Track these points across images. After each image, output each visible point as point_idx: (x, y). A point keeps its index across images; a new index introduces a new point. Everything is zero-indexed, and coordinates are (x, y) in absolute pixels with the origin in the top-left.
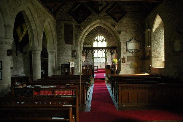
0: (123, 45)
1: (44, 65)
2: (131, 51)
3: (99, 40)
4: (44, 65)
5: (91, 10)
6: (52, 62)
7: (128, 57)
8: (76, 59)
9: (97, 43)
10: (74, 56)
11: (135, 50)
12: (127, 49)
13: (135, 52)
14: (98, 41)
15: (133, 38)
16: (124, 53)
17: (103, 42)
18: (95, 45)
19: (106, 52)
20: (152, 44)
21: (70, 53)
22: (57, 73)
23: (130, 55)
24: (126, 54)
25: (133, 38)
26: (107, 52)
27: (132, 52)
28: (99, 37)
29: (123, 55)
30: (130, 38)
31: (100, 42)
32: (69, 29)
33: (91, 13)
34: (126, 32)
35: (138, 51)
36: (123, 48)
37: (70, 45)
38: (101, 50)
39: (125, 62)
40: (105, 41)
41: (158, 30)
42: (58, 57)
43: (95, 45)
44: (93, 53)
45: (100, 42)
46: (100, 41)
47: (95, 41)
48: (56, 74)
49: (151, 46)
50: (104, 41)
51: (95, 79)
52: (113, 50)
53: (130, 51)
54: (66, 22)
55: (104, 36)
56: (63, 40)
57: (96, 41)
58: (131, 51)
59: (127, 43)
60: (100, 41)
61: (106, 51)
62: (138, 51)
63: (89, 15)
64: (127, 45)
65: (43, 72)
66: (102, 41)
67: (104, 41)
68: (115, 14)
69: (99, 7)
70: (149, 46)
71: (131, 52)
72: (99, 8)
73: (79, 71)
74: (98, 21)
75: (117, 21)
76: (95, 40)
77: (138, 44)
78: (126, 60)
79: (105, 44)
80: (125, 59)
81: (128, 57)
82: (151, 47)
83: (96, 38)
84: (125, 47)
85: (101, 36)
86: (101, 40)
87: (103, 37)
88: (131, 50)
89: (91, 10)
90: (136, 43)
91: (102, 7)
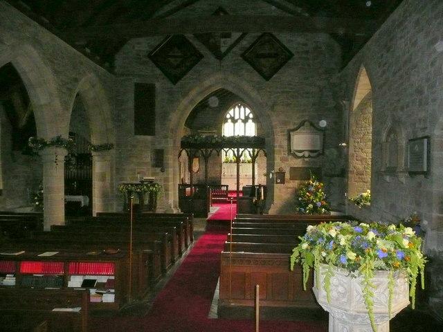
0: (280, 140)
1: (79, 183)
2: (301, 155)
3: (236, 117)
4: (79, 183)
5: (203, 50)
6: (103, 178)
7: (293, 169)
8: (162, 171)
9: (232, 124)
10: (159, 160)
11: (311, 151)
12: (290, 150)
13: (309, 156)
14: (234, 121)
15: (305, 122)
16: (283, 160)
17: (247, 124)
18: (228, 130)
19: (253, 154)
20: (351, 140)
21: (148, 157)
22: (116, 208)
23: (298, 163)
24: (287, 160)
25: (305, 122)
26: (257, 155)
27: (303, 157)
28: (237, 109)
29: (278, 164)
30: (298, 122)
31: (240, 124)
32: (145, 96)
33: (201, 56)
34: (288, 105)
35: (319, 155)
36: (281, 146)
37: (149, 138)
38: (226, 149)
39: (283, 182)
40: (254, 120)
41: (366, 104)
42: (118, 168)
43: (228, 130)
44: (219, 154)
45: (240, 124)
46: (240, 121)
47: (226, 120)
48: (113, 209)
49: (348, 143)
50: (250, 121)
51: (208, 221)
52: (241, 150)
53: (297, 153)
54: (136, 80)
55: (250, 107)
56: (130, 124)
57: (229, 121)
58: (301, 155)
59: (292, 133)
60: (240, 121)
61: (254, 151)
62: (319, 155)
63: (195, 63)
64: (289, 139)
65: (82, 202)
66: (245, 121)
67: (250, 121)
68: (263, 61)
69: (223, 40)
70: (344, 144)
71: (300, 157)
72: (222, 44)
73: (169, 202)
74: (219, 76)
75: (267, 78)
76: (228, 116)
77: (318, 137)
78: (287, 176)
79: (251, 130)
80: (284, 173)
81: (293, 169)
82: (348, 146)
83: (231, 112)
84: (285, 143)
85: (242, 109)
86: (243, 117)
87: (248, 111)
88: (300, 151)
89: (203, 50)
90: (312, 133)
91: (230, 41)
